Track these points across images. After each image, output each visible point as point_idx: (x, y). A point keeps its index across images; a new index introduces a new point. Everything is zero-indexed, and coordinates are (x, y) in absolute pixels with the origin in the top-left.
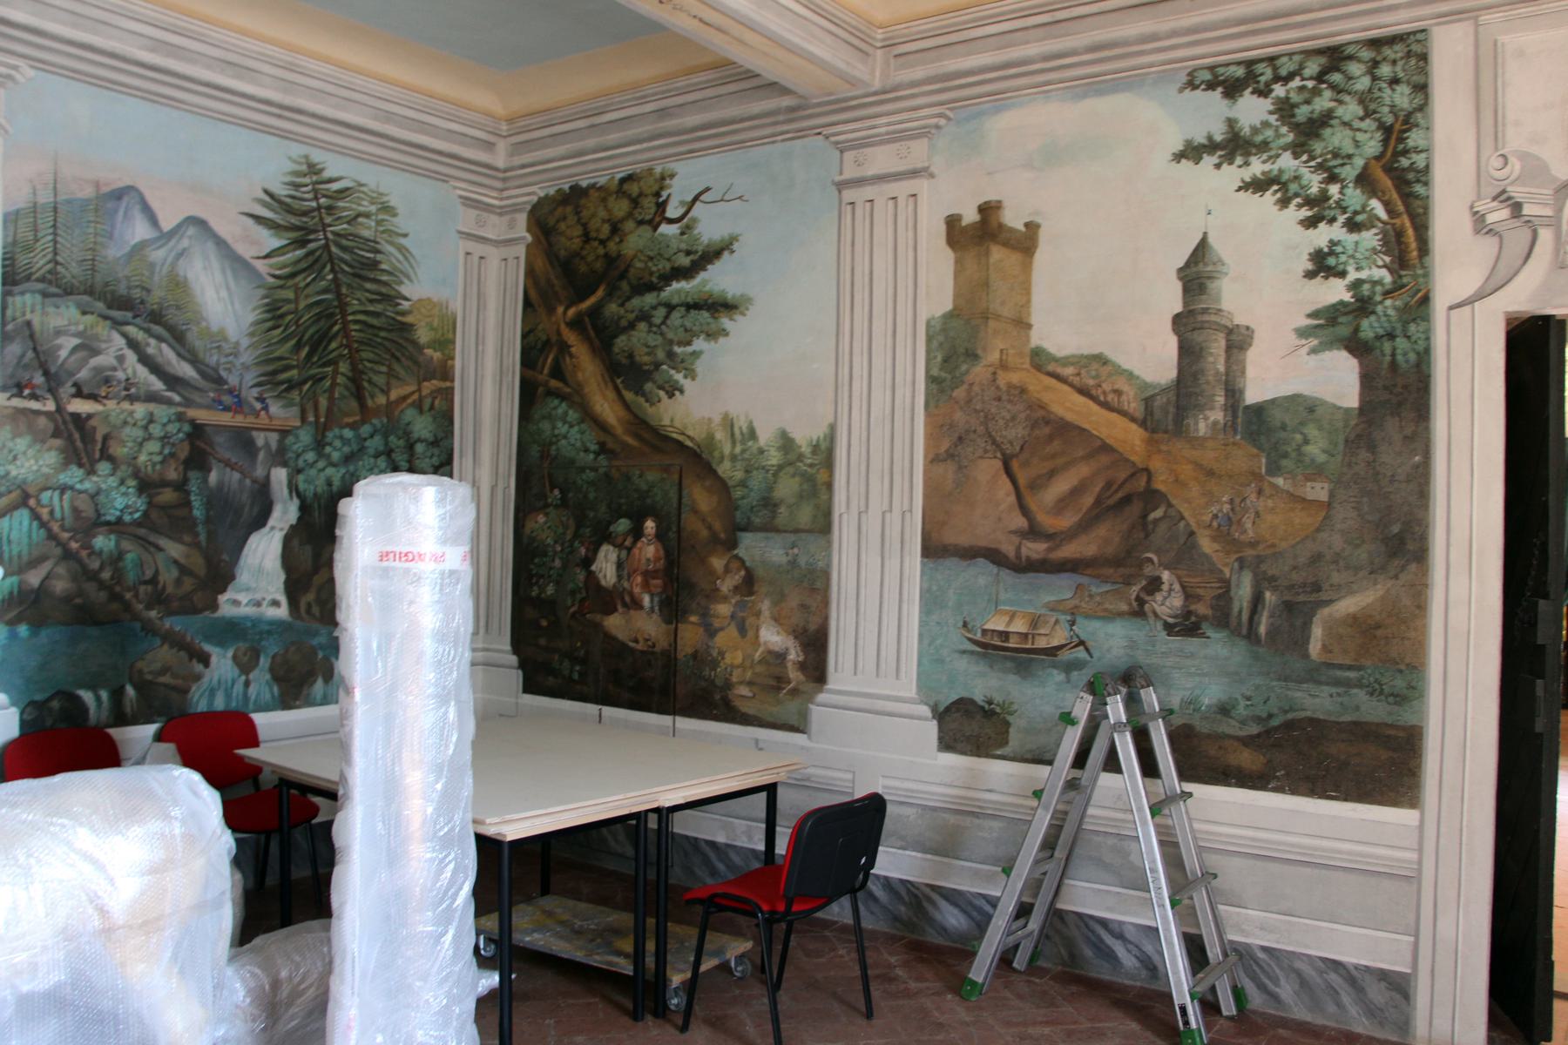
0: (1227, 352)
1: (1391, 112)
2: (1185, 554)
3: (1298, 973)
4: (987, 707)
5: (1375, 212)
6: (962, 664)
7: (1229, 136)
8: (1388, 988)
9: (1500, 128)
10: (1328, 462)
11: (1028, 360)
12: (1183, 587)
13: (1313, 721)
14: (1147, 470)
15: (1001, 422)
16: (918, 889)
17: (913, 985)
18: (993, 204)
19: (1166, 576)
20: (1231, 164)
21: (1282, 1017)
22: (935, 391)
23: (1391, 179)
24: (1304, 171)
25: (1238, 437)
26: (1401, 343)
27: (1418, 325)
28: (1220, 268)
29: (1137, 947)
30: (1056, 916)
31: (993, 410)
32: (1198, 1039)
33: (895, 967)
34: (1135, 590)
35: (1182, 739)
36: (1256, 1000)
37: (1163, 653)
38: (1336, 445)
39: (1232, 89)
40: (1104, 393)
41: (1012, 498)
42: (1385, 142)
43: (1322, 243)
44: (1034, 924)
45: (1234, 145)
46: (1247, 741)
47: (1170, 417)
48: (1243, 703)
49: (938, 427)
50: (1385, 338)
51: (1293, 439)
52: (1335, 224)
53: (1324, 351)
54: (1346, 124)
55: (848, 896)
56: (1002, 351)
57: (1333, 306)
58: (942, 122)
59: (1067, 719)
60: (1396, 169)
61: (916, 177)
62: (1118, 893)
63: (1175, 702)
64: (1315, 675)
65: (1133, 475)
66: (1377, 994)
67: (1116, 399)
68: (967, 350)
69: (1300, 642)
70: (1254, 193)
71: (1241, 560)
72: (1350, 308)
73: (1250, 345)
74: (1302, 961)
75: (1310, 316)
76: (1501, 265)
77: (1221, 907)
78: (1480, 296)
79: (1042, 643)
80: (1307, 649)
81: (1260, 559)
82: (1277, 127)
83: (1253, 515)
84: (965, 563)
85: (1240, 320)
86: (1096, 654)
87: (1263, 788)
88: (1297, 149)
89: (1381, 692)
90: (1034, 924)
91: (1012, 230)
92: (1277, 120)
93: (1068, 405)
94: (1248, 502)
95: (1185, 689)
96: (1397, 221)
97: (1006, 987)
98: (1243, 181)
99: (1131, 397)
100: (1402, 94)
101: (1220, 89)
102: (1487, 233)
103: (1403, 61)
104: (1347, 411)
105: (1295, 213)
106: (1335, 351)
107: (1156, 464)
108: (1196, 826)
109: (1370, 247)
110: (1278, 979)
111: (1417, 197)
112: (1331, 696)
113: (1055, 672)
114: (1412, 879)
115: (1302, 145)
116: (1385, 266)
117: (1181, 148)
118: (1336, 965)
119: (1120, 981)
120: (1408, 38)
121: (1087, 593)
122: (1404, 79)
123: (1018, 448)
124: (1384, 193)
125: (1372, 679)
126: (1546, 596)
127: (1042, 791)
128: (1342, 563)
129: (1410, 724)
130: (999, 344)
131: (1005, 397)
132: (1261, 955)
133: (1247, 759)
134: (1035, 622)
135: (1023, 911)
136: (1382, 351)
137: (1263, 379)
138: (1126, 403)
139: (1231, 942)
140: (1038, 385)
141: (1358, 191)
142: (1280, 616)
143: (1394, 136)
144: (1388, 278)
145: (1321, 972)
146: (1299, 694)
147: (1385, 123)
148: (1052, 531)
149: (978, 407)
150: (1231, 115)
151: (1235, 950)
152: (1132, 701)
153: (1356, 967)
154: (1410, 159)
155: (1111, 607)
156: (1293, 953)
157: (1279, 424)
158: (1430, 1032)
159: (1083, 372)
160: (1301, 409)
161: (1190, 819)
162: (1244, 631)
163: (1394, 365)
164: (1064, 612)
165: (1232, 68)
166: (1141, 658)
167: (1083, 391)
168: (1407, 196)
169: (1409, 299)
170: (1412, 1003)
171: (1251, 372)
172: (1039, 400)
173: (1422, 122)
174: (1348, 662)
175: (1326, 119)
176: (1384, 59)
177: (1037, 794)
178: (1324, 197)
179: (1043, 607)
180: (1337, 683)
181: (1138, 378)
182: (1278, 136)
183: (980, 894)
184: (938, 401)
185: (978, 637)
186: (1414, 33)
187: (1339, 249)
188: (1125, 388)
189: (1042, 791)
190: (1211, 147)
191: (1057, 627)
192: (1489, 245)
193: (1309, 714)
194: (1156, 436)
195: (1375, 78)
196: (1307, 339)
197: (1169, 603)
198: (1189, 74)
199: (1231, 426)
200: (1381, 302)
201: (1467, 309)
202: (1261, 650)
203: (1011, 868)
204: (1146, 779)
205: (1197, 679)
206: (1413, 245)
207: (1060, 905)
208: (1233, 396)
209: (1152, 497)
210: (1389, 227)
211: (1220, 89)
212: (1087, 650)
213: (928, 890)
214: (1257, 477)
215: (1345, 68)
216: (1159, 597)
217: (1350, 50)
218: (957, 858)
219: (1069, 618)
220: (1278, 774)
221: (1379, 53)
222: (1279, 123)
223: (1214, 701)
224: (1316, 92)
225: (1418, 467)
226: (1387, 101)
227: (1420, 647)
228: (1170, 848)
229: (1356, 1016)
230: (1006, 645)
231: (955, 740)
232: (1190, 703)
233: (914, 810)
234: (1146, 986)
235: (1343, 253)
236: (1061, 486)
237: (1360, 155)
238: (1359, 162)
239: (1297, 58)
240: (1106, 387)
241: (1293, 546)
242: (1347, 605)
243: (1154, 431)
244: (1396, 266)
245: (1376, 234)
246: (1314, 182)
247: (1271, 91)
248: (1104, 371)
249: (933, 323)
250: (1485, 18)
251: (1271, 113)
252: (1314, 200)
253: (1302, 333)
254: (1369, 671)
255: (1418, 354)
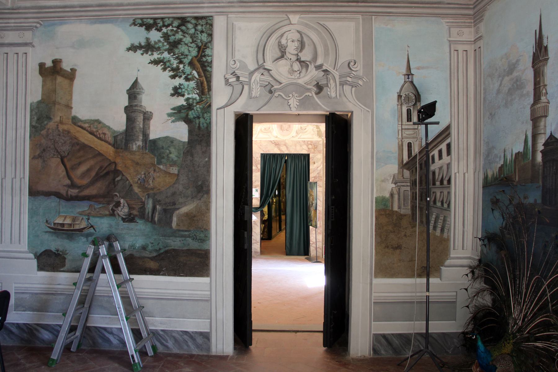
0: (143, 120)
1: (200, 42)
2: (129, 193)
3: (174, 337)
4: (56, 252)
5: (194, 75)
6: (46, 237)
7: (147, 44)
8: (203, 338)
9: (234, 52)
10: (177, 160)
11: (71, 121)
12: (128, 205)
13: (174, 250)
14: (115, 163)
15: (60, 144)
16: (31, 326)
17: (28, 365)
18: (58, 60)
19: (122, 201)
20: (147, 53)
21: (170, 353)
22: (34, 131)
23: (200, 64)
24: (172, 59)
25: (147, 151)
26: (202, 120)
27: (207, 114)
28: (142, 90)
29: (118, 336)
30: (87, 329)
31: (57, 139)
32: (138, 366)
33: (21, 359)
34: (111, 206)
35: (129, 260)
36: (160, 349)
37: (121, 229)
38: (180, 154)
39: (148, 28)
40: (99, 134)
41: (65, 173)
42: (198, 52)
43: (177, 84)
44: (78, 333)
45: (148, 47)
46: (152, 259)
47: (123, 143)
48: (150, 245)
49: (34, 146)
50: (196, 118)
51: (166, 152)
52: (181, 78)
53: (176, 121)
54: (186, 44)
55: (323, 330)
56: (61, 117)
57: (180, 106)
58: (38, 25)
59: (85, 255)
60: (202, 61)
61: (27, 46)
62: (110, 317)
63: (127, 246)
64: (175, 234)
65: (110, 164)
66: (200, 340)
67: (104, 136)
68: (47, 116)
69: (169, 223)
70: (154, 65)
71: (148, 195)
72: (185, 107)
73: (152, 119)
74: (175, 332)
75: (172, 109)
76: (233, 96)
77: (146, 318)
78: (226, 106)
79: (77, 227)
80: (171, 225)
81: (155, 194)
82: (163, 42)
83: (152, 179)
84: (46, 198)
85: (148, 109)
86: (97, 230)
87: (159, 274)
88: (170, 51)
89: (196, 239)
90: (78, 333)
91: (65, 71)
92: (163, 40)
93: (86, 138)
94: (151, 174)
95: (130, 241)
96: (201, 79)
97: (67, 359)
98: (151, 60)
99: (109, 136)
100: (204, 36)
101: (144, 27)
102: (229, 85)
103: (205, 26)
104: (184, 142)
105: (168, 73)
106: (180, 122)
107: (118, 160)
108: (136, 290)
109: (192, 87)
110: (168, 340)
111: (208, 71)
112: (180, 241)
113: (82, 238)
114: (208, 300)
115: (171, 50)
116: (197, 94)
117: (130, 46)
118: (186, 333)
119: (112, 349)
120: (207, 18)
121: (93, 208)
122: (205, 31)
123: (67, 154)
124: (197, 69)
125: (193, 235)
126: (247, 205)
127: (76, 283)
128: (182, 195)
129: (205, 249)
130: (60, 114)
131: (62, 134)
132: (161, 333)
133: (153, 265)
134: (74, 219)
135: (73, 329)
136: (195, 122)
137: (156, 131)
138: (107, 138)
139: (150, 329)
140: (74, 130)
141: (189, 67)
142: (162, 214)
143: (201, 50)
144: (198, 98)
145: (181, 336)
146: (169, 241)
147: (199, 45)
148: (80, 185)
149: (51, 138)
150: (148, 36)
151: (153, 332)
152: (110, 248)
153: (193, 332)
154: (206, 58)
155: (102, 213)
156: (172, 330)
157: (161, 147)
158: (216, 349)
159: (91, 126)
160: (169, 142)
161: (133, 288)
162: (150, 220)
163: (199, 127)
164: (85, 215)
165: (149, 20)
166: (114, 231)
167: (92, 133)
168: (205, 71)
169: (204, 105)
170: (210, 341)
171: (152, 128)
172: (75, 136)
173: (210, 46)
174: (185, 229)
175: (179, 42)
176: (199, 24)
177: (75, 284)
178: (178, 68)
179: (77, 214)
180: (182, 236)
181: (112, 129)
182: (163, 46)
183: (57, 325)
184: (35, 135)
185: (52, 226)
186: (209, 17)
187: (182, 87)
188: (107, 133)
189: (76, 283)
190: (140, 47)
191: (83, 221)
192: (230, 88)
193: (173, 248)
194: (118, 150)
195: (196, 30)
196: (171, 117)
197: (123, 211)
198: (134, 20)
199: (144, 147)
200: (196, 106)
201: (222, 110)
202: (156, 226)
203: (66, 313)
204: (115, 275)
205: (134, 238)
206: (206, 87)
207: (88, 325)
208: (146, 136)
209: (117, 172)
210: (199, 80)
211: (144, 27)
212: (94, 229)
213: (36, 326)
214: (153, 165)
215: (186, 25)
216: (120, 209)
217: (189, 19)
218: (47, 312)
219: (87, 217)
220: (163, 269)
221: (197, 21)
222: (164, 41)
223: (140, 245)
224: (177, 32)
225: (207, 162)
226: (200, 38)
227: (208, 223)
228: (126, 299)
229: (194, 349)
230: (63, 228)
231: (44, 266)
232: (132, 246)
233: (28, 295)
234: (122, 350)
235: (184, 88)
236: (83, 168)
237: (190, 55)
238: (190, 58)
239: (171, 19)
240: (100, 132)
241: (166, 189)
242: (184, 210)
243: (117, 148)
244: (201, 94)
245: (194, 83)
246: (175, 63)
247: (162, 30)
248: (100, 126)
249: (33, 105)
250: (230, 15)
251: (161, 37)
252: (175, 69)
253: (170, 115)
254: (192, 232)
255: (207, 124)
